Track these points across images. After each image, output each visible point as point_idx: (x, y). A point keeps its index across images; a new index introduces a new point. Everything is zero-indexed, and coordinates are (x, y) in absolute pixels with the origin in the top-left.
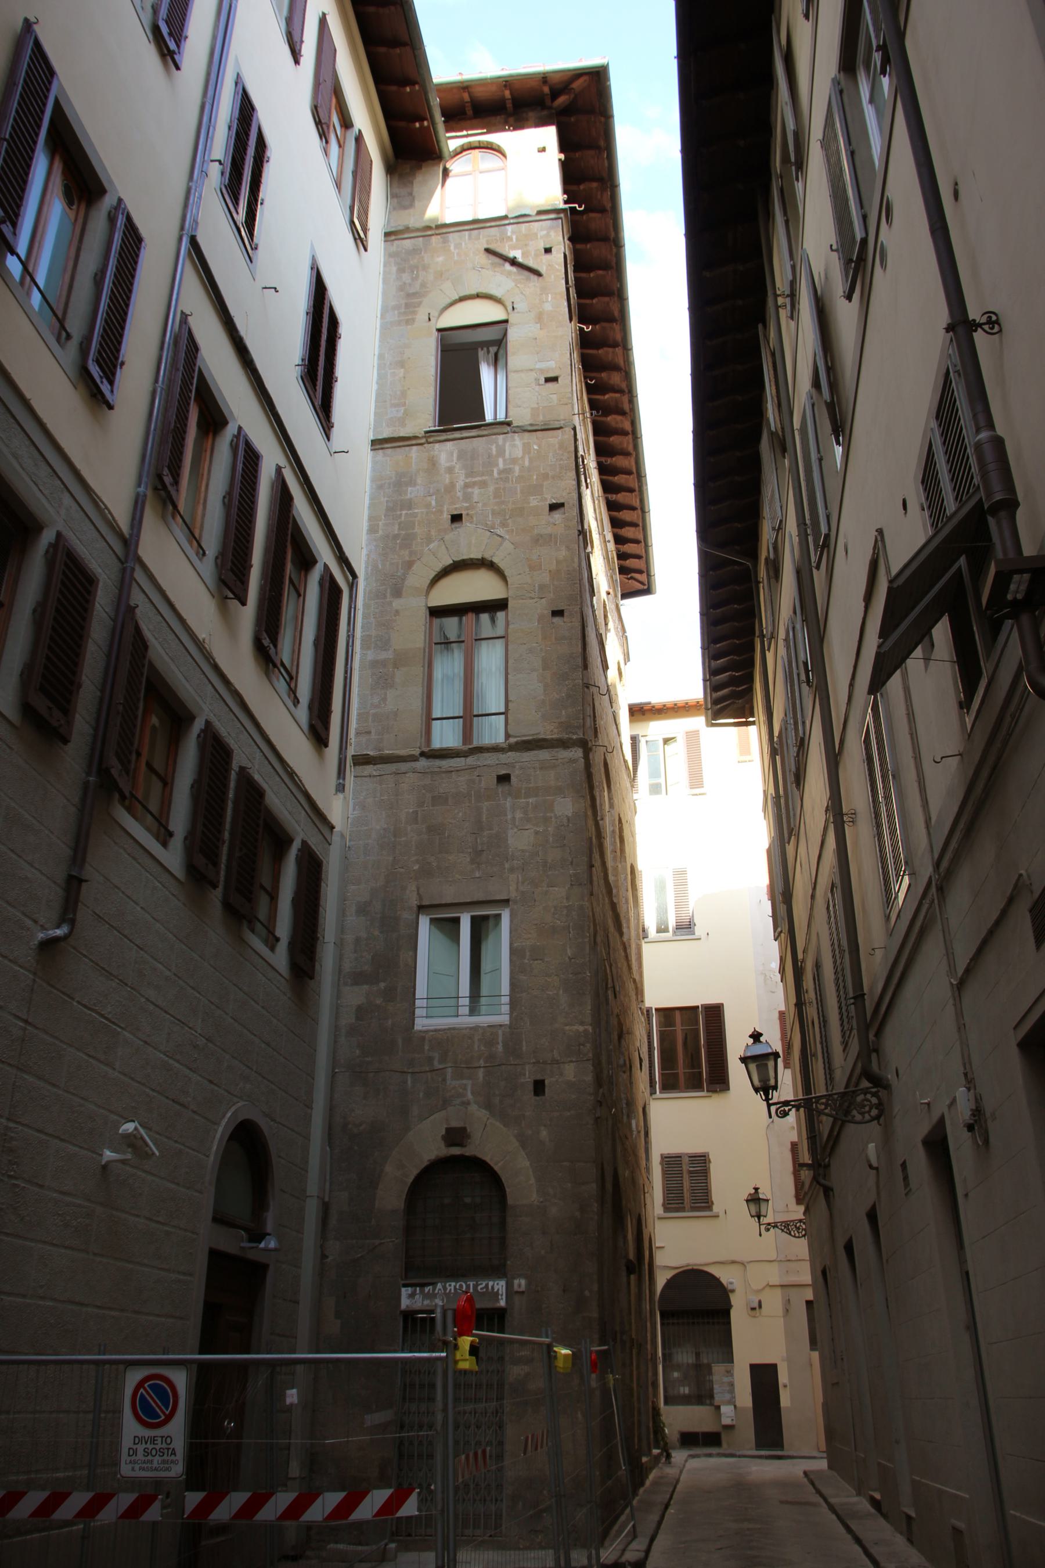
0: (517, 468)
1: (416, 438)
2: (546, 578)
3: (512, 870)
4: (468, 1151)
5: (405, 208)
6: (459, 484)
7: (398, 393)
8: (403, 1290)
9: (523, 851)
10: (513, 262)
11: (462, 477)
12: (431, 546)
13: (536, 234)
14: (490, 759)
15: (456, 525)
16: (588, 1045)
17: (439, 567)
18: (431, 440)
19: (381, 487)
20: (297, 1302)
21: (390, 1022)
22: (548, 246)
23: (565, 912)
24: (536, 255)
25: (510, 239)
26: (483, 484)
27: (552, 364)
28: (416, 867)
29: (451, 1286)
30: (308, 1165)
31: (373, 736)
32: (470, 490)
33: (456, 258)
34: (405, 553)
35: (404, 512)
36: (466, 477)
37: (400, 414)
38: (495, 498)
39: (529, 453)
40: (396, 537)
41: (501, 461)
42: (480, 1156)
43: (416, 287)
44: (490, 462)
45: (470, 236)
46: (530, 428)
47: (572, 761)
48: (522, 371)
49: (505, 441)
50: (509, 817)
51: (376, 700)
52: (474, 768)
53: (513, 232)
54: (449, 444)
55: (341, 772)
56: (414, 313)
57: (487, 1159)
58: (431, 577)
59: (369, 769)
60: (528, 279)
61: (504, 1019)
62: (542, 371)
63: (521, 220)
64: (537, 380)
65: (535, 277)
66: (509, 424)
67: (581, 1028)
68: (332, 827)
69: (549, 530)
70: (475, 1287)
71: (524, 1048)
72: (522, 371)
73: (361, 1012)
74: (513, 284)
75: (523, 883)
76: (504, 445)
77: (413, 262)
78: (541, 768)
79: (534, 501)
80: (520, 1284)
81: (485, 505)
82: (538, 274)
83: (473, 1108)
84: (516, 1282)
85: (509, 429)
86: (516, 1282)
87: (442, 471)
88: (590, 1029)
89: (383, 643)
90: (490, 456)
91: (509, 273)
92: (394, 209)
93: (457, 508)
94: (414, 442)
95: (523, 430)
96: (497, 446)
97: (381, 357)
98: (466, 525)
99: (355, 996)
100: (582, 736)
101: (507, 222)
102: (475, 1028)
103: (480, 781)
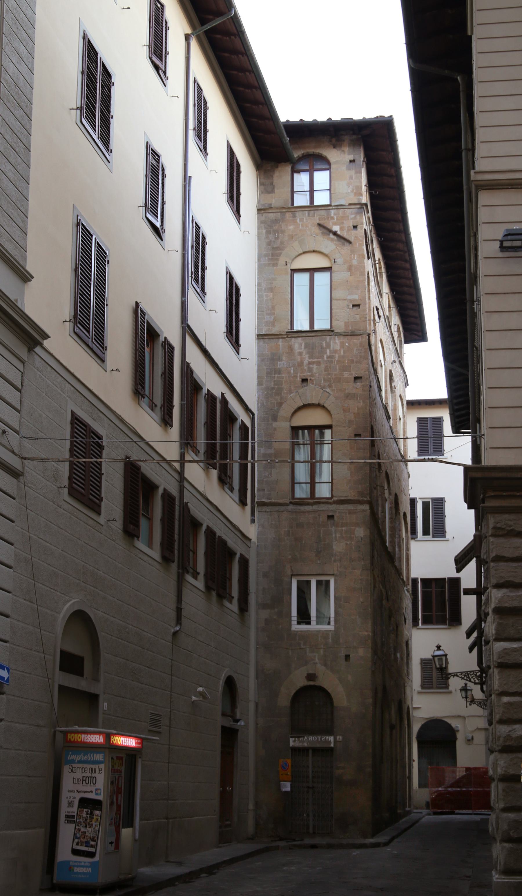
0: (337, 356)
1: (281, 335)
2: (352, 417)
3: (335, 561)
4: (317, 683)
5: (269, 193)
6: (306, 362)
7: (270, 307)
8: (291, 739)
9: (340, 552)
10: (335, 233)
11: (307, 358)
12: (292, 395)
13: (348, 217)
14: (324, 507)
15: (305, 384)
16: (370, 641)
17: (296, 407)
18: (290, 336)
19: (263, 360)
20: (248, 743)
21: (280, 626)
22: (355, 225)
23: (360, 581)
24: (348, 230)
25: (333, 218)
26: (319, 363)
27: (356, 297)
28: (290, 557)
29: (311, 738)
30: (250, 689)
31: (266, 492)
32: (311, 366)
33: (301, 228)
34: (278, 398)
35: (276, 375)
36: (309, 358)
37: (272, 319)
38: (325, 371)
39: (343, 348)
40: (273, 389)
41: (328, 351)
42: (322, 686)
43: (277, 244)
44: (322, 351)
45: (309, 214)
46: (344, 334)
47: (364, 511)
48: (340, 300)
49: (330, 339)
50: (334, 535)
51: (266, 474)
52: (316, 511)
53: (335, 214)
54: (300, 339)
55: (253, 513)
56: (277, 260)
57: (325, 687)
58: (292, 412)
59: (265, 508)
60: (343, 244)
61: (332, 627)
62: (351, 301)
63: (339, 207)
64: (348, 306)
65: (348, 244)
66: (332, 331)
67: (366, 633)
68: (250, 540)
69: (354, 391)
70: (321, 739)
71: (341, 641)
72: (340, 300)
73: (267, 621)
74: (335, 247)
75: (340, 567)
76: (330, 342)
77: (276, 228)
78: (349, 513)
79: (346, 375)
80: (340, 738)
81: (319, 375)
82: (350, 242)
83: (319, 666)
84: (338, 737)
85: (332, 333)
86: (338, 737)
87: (296, 354)
88: (370, 634)
89: (269, 445)
90: (322, 348)
91: (332, 240)
92: (262, 193)
93: (306, 375)
94: (280, 337)
95: (339, 334)
96: (326, 342)
97: (259, 285)
98: (311, 386)
99: (265, 614)
100: (369, 499)
101: (331, 208)
102: (319, 631)
103: (319, 518)
